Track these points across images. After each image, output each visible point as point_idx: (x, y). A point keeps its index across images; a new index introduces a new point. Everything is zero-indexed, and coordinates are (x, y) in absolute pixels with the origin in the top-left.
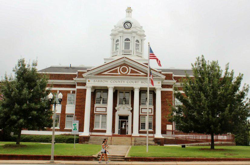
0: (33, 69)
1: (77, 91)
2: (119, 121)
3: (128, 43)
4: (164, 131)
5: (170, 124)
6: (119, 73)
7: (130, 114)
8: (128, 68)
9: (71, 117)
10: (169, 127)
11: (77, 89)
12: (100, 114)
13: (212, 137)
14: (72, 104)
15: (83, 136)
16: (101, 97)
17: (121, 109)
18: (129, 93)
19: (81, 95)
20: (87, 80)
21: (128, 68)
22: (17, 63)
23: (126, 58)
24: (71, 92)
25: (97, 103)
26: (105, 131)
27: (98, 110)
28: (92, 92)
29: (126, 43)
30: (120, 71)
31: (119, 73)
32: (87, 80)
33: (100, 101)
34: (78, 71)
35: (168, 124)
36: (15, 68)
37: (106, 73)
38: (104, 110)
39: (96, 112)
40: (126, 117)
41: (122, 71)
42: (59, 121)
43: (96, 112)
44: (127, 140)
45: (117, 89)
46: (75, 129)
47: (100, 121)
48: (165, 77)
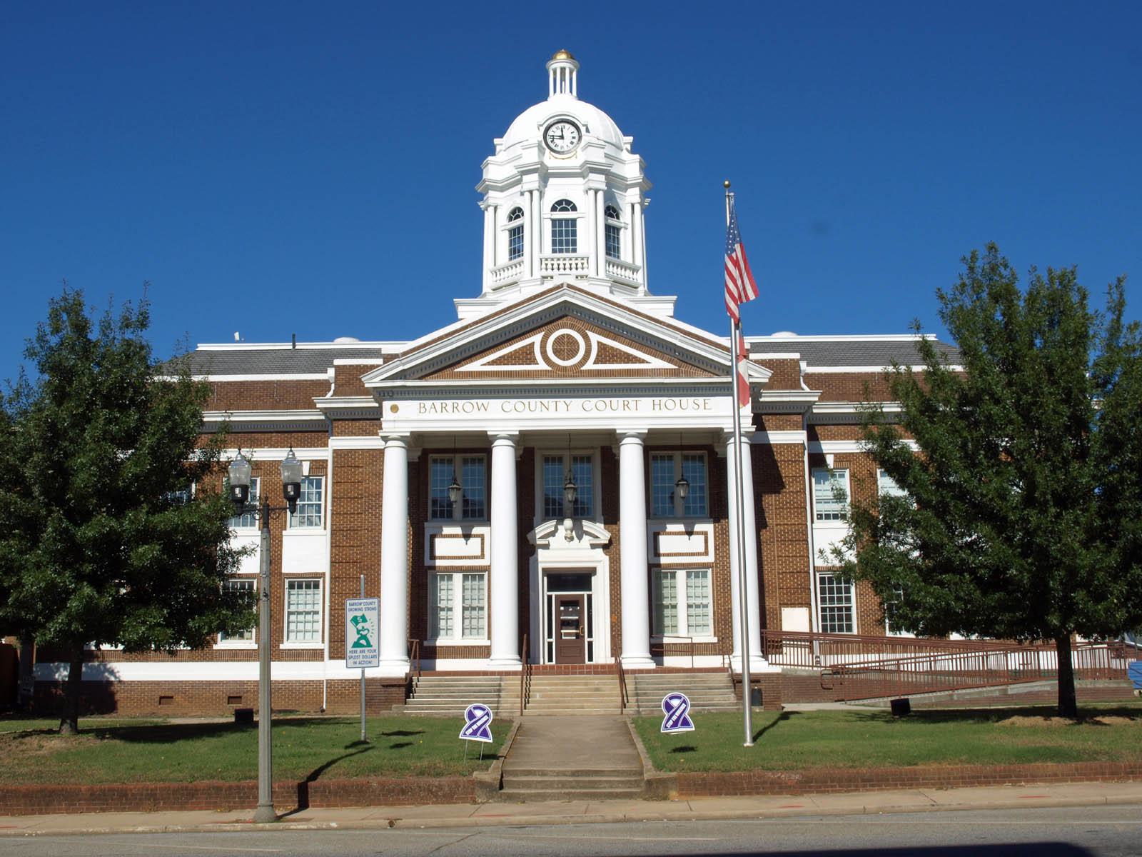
0: (129, 343)
1: (334, 462)
3: (567, 220)
4: (771, 643)
5: (801, 605)
6: (542, 366)
7: (600, 561)
8: (586, 338)
9: (308, 587)
10: (795, 619)
11: (338, 454)
13: (1065, 660)
14: (311, 524)
15: (382, 679)
17: (558, 541)
18: (588, 459)
19: (358, 476)
20: (387, 405)
21: (586, 338)
22: (44, 316)
23: (569, 286)
25: (434, 515)
26: (484, 652)
29: (560, 220)
30: (544, 353)
31: (542, 366)
32: (387, 405)
34: (337, 362)
35: (787, 605)
36: (34, 340)
40: (582, 579)
41: (556, 352)
44: (597, 690)
45: (531, 444)
46: (363, 642)
47: (457, 605)
48: (769, 373)
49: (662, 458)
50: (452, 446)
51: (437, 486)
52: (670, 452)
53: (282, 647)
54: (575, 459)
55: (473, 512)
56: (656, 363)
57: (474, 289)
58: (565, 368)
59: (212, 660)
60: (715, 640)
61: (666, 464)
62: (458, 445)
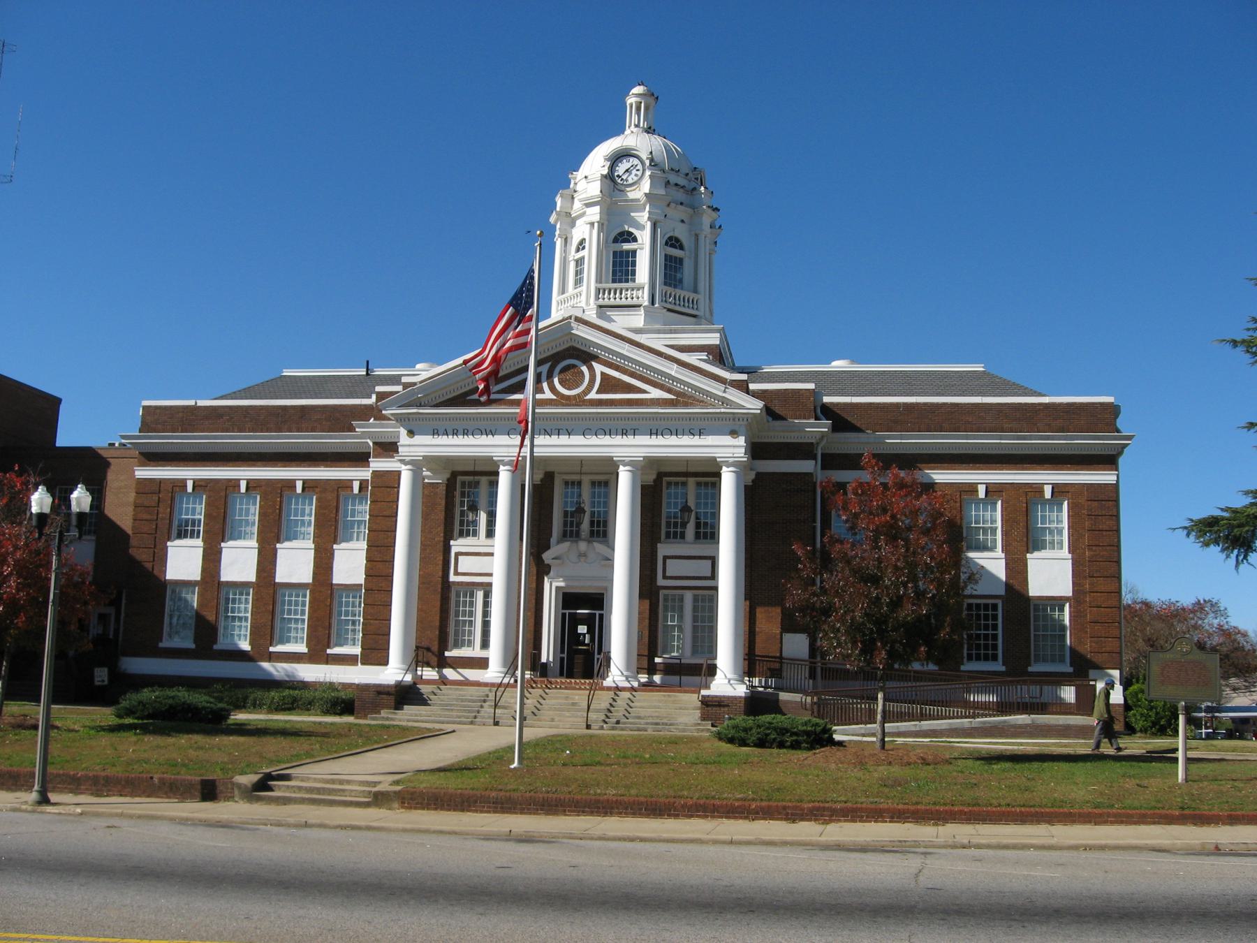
2: (564, 615)
11: (376, 474)
12: (473, 584)
16: (686, 509)
21: (591, 369)
24: (299, 486)
25: (668, 535)
27: (674, 568)
28: (643, 487)
33: (684, 525)
34: (379, 389)
37: (655, 393)
38: (703, 568)
39: (665, 577)
42: (306, 617)
43: (665, 577)
44: (574, 704)
45: (550, 469)
49: (677, 484)
50: (471, 469)
51: (669, 508)
52: (684, 479)
53: (161, 645)
54: (593, 483)
55: (706, 534)
56: (655, 393)
57: (549, 316)
58: (568, 397)
59: (327, 663)
60: (193, 646)
61: (680, 490)
62: (691, 470)
